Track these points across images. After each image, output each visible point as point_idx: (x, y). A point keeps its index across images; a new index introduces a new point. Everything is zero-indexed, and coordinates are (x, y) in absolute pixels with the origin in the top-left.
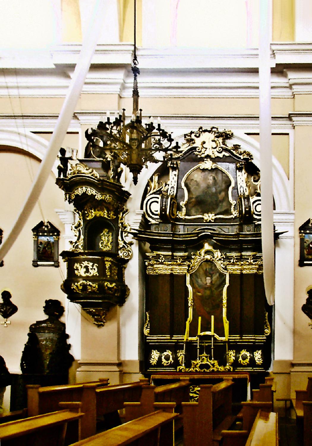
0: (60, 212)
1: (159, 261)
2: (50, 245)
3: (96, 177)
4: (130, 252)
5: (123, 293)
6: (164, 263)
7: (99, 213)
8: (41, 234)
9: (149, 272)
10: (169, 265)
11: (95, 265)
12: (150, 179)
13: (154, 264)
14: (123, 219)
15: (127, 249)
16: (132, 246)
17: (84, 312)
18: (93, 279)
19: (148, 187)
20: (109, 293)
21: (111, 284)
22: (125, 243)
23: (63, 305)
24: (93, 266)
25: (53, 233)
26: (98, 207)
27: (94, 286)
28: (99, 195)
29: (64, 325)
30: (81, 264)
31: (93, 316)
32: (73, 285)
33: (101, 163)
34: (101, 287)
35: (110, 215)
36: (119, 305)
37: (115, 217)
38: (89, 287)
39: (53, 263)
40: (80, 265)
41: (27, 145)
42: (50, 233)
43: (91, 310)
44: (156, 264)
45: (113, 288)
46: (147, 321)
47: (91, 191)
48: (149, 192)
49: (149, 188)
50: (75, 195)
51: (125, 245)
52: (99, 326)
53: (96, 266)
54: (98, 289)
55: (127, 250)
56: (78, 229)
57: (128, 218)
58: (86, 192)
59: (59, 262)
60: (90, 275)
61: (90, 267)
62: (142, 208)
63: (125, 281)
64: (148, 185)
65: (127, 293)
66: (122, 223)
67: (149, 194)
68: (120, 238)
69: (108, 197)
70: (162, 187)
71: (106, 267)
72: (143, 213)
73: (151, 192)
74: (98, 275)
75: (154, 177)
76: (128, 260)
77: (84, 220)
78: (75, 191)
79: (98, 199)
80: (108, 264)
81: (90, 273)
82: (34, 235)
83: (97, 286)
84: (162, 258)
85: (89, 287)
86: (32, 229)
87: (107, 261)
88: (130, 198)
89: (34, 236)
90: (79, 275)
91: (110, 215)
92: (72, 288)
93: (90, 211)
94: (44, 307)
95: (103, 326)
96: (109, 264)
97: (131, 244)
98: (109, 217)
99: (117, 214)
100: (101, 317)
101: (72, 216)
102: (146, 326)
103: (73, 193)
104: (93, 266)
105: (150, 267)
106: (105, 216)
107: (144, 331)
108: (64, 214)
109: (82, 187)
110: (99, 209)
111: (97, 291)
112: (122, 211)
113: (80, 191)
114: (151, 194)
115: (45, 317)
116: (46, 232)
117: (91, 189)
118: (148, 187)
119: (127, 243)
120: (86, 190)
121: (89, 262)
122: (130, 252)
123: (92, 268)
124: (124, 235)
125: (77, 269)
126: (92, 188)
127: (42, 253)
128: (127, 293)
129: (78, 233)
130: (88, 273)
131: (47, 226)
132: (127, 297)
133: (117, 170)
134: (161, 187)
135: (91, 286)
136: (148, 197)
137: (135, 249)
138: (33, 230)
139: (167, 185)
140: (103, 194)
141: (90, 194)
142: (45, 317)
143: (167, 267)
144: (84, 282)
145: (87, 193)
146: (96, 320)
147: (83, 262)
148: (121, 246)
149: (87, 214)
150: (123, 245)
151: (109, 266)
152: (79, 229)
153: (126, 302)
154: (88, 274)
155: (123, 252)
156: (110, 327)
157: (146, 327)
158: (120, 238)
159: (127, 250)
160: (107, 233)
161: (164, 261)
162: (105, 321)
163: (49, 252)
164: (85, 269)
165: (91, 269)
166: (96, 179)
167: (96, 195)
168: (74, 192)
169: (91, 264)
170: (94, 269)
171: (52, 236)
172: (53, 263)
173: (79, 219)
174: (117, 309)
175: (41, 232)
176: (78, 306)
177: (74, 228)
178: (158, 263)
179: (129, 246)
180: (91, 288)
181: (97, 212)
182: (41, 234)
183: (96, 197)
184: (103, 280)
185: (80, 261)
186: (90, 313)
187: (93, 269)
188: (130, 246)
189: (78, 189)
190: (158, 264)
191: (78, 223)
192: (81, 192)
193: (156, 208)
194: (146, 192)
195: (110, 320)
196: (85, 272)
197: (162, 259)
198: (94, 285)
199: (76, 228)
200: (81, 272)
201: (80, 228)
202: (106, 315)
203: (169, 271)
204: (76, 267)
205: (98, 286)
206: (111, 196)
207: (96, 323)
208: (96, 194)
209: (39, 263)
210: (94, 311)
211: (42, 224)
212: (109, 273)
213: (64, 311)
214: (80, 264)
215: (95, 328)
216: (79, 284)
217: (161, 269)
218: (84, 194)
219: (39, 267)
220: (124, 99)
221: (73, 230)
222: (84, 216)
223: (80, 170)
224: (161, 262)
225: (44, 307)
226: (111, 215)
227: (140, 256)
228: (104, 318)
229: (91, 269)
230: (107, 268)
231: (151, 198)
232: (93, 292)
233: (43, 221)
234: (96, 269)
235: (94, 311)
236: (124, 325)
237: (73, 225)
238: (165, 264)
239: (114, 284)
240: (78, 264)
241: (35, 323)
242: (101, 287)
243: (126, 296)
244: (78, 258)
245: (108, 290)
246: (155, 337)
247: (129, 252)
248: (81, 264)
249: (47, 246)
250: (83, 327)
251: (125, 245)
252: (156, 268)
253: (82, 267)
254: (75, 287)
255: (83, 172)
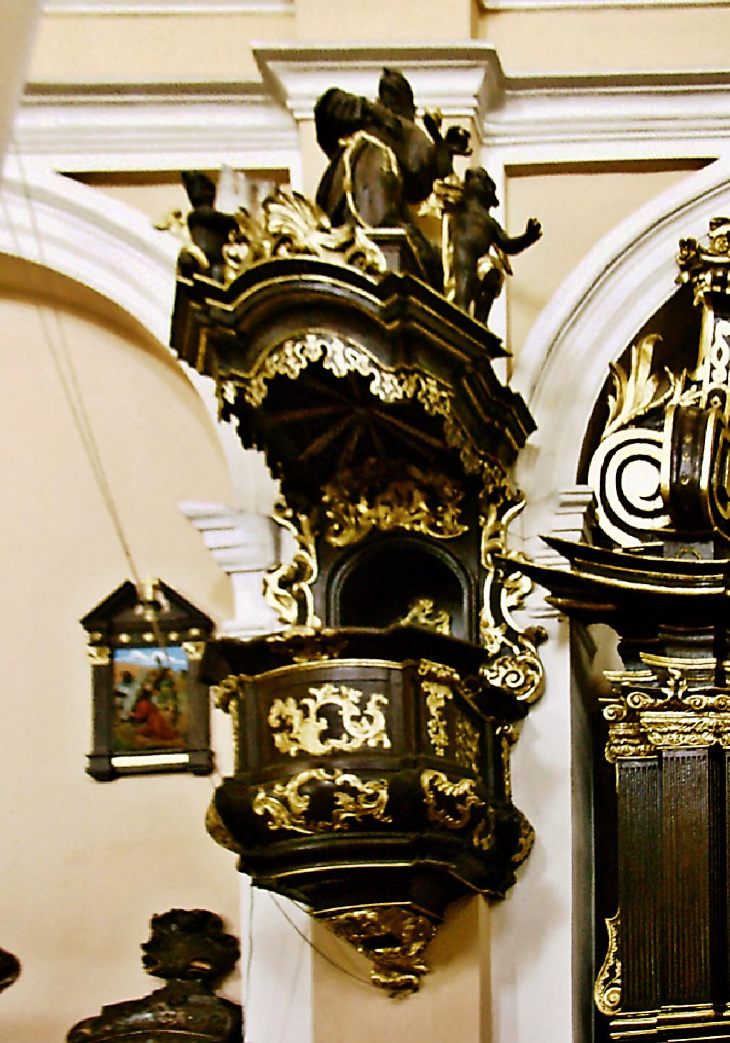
0: (208, 517)
1: (665, 696)
2: (172, 684)
3: (371, 270)
4: (533, 667)
5: (500, 848)
6: (686, 701)
7: (386, 517)
8: (124, 638)
9: (617, 749)
10: (709, 708)
11: (375, 697)
12: (619, 361)
13: (642, 709)
14: (502, 533)
15: (520, 659)
16: (541, 648)
17: (329, 937)
18: (363, 762)
19: (611, 398)
20: (445, 827)
21: (454, 780)
22: (511, 634)
23: (233, 932)
24: (362, 705)
25: (183, 629)
26: (383, 489)
27: (370, 791)
28: (388, 377)
29: (236, 1011)
30: (305, 701)
31: (369, 945)
32: (261, 795)
33: (396, 255)
34: (406, 799)
35: (441, 519)
36: (486, 896)
37: (466, 528)
38: (343, 798)
39: (184, 758)
40: (299, 707)
41: (37, 234)
42: (168, 631)
43: (356, 914)
44: (652, 708)
45: (462, 798)
46: (610, 956)
47: (346, 356)
48: (614, 419)
49: (612, 402)
50: (266, 381)
51: (509, 643)
52: (396, 990)
53: (378, 703)
54: (390, 808)
55: (519, 664)
56: (295, 587)
57: (522, 530)
58: (322, 359)
59: (212, 754)
60: (347, 748)
61: (348, 711)
62: (582, 478)
63: (510, 796)
64: (609, 389)
65: (522, 840)
66: (494, 551)
67: (617, 424)
68: (486, 614)
69: (433, 390)
70: (673, 394)
71: (428, 709)
72: (590, 498)
73: (623, 418)
74: (387, 744)
75: (634, 350)
76: (525, 708)
77: (323, 550)
78: (268, 363)
79: (382, 397)
80: (437, 697)
81: (351, 737)
82: (93, 644)
83: (384, 795)
84: (677, 682)
85: (343, 798)
86: (82, 617)
87: (431, 677)
88: (531, 447)
89: (93, 650)
90: (293, 754)
91: (441, 519)
92: (259, 811)
93: (351, 508)
94: (144, 947)
95: (416, 989)
96: (441, 696)
97: (538, 637)
98: (439, 530)
99: (471, 513)
100: (405, 951)
101: (266, 536)
102: (607, 975)
103: (259, 372)
104: (362, 705)
105: (621, 729)
106: (417, 528)
107: (597, 998)
108: (226, 523)
109: (303, 338)
110: (389, 497)
111: (385, 815)
112: (493, 498)
113: (291, 360)
114: (623, 427)
115: (145, 985)
116: (147, 627)
117: (349, 345)
118: (611, 398)
119: (516, 634)
120: (320, 353)
121: (344, 689)
122: (533, 667)
123: (357, 712)
124: (507, 600)
125: (285, 726)
126: (352, 341)
127: (132, 719)
128: (522, 840)
129: (295, 605)
130: (338, 737)
131: (155, 605)
132: (520, 863)
133: (475, 267)
134: (667, 395)
135: (354, 792)
136: (611, 438)
137: (555, 662)
138: (89, 622)
139: (694, 387)
140: (408, 373)
141: (344, 373)
142: (145, 985)
143: (697, 720)
144: (320, 774)
145: (326, 366)
146: (385, 966)
147: (312, 691)
148: (493, 649)
149: (332, 522)
150: (503, 645)
151: (442, 703)
152: (301, 591)
153: (517, 886)
154: (340, 744)
155: (503, 672)
156: (448, 992)
157: (606, 981)
158: (486, 614)
159: (519, 664)
160: (428, 616)
161: (686, 694)
162: (422, 967)
163: (167, 715)
164: (323, 721)
165: (355, 719)
166: (370, 278)
167: (372, 377)
168: (263, 368)
169: (355, 695)
170: (371, 719)
171: (178, 644)
172: (184, 758)
173: (298, 545)
174: (476, 915)
175: (127, 632)
176: (298, 912)
177: (274, 587)
178: (660, 701)
179: (527, 644)
180: (356, 802)
181: (382, 510)
182: (124, 638)
183: (374, 388)
184: (415, 764)
185: (299, 687)
186: (350, 929)
187: (364, 719)
188: (536, 645)
189: (280, 348)
190: (660, 709)
191: (295, 565)
192: (299, 361)
193: (643, 483)
194: (600, 416)
195: (447, 960)
196: (324, 736)
197: (677, 687)
198: (368, 788)
199: (285, 583)
200: (308, 736)
201: (304, 586)
202: (428, 939)
203: (711, 738)
204: (279, 718)
205: (389, 792)
206: (446, 389)
207: (383, 980)
208: (376, 372)
209: (118, 762)
210: (371, 915)
211: (127, 595)
212: (442, 732)
213: (237, 955)
214: (298, 700)
215: (380, 1004)
216: (293, 784)
217: (673, 728)
218: (316, 370)
219: (122, 782)
220: (498, 18)
221: (270, 595)
222: (321, 529)
223: (285, 231)
224: (675, 697)
225: (144, 947)
226: (448, 518)
227: (574, 688)
228: (419, 951)
229: (355, 719)
230: (433, 711)
231: (619, 447)
232: (367, 823)
233: (133, 581)
234: (380, 721)
235: (371, 915)
236: (511, 979)
237: (270, 572)
238: (688, 708)
239: (465, 786)
240: (291, 701)
241: (97, 1013)
242: (406, 799)
243: (517, 857)
244: (287, 673)
245: (438, 808)
246: (645, 1018)
247: (530, 672)
248: (305, 701)
249: (157, 686)
250: (320, 1004)
251: (509, 643)
252: (650, 724)
253: (306, 715)
254: (273, 806)
255: (301, 242)
